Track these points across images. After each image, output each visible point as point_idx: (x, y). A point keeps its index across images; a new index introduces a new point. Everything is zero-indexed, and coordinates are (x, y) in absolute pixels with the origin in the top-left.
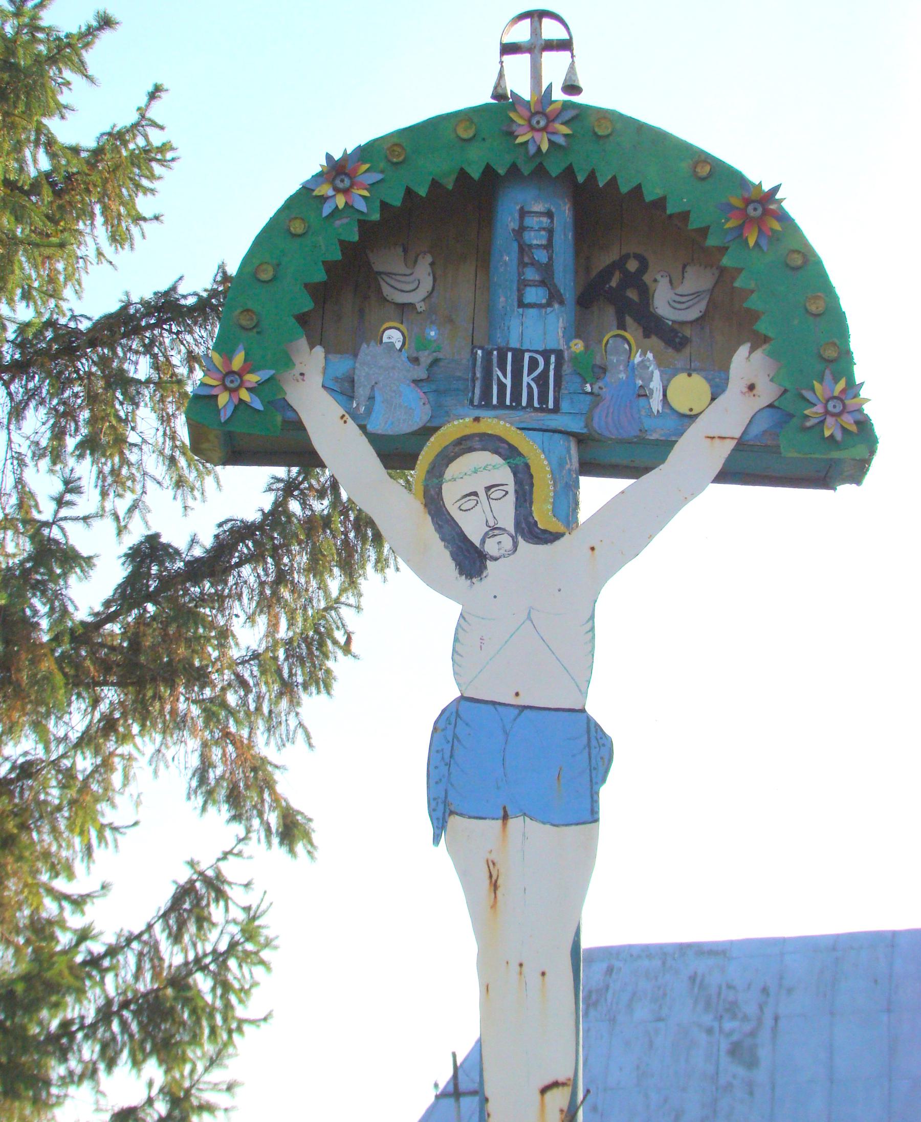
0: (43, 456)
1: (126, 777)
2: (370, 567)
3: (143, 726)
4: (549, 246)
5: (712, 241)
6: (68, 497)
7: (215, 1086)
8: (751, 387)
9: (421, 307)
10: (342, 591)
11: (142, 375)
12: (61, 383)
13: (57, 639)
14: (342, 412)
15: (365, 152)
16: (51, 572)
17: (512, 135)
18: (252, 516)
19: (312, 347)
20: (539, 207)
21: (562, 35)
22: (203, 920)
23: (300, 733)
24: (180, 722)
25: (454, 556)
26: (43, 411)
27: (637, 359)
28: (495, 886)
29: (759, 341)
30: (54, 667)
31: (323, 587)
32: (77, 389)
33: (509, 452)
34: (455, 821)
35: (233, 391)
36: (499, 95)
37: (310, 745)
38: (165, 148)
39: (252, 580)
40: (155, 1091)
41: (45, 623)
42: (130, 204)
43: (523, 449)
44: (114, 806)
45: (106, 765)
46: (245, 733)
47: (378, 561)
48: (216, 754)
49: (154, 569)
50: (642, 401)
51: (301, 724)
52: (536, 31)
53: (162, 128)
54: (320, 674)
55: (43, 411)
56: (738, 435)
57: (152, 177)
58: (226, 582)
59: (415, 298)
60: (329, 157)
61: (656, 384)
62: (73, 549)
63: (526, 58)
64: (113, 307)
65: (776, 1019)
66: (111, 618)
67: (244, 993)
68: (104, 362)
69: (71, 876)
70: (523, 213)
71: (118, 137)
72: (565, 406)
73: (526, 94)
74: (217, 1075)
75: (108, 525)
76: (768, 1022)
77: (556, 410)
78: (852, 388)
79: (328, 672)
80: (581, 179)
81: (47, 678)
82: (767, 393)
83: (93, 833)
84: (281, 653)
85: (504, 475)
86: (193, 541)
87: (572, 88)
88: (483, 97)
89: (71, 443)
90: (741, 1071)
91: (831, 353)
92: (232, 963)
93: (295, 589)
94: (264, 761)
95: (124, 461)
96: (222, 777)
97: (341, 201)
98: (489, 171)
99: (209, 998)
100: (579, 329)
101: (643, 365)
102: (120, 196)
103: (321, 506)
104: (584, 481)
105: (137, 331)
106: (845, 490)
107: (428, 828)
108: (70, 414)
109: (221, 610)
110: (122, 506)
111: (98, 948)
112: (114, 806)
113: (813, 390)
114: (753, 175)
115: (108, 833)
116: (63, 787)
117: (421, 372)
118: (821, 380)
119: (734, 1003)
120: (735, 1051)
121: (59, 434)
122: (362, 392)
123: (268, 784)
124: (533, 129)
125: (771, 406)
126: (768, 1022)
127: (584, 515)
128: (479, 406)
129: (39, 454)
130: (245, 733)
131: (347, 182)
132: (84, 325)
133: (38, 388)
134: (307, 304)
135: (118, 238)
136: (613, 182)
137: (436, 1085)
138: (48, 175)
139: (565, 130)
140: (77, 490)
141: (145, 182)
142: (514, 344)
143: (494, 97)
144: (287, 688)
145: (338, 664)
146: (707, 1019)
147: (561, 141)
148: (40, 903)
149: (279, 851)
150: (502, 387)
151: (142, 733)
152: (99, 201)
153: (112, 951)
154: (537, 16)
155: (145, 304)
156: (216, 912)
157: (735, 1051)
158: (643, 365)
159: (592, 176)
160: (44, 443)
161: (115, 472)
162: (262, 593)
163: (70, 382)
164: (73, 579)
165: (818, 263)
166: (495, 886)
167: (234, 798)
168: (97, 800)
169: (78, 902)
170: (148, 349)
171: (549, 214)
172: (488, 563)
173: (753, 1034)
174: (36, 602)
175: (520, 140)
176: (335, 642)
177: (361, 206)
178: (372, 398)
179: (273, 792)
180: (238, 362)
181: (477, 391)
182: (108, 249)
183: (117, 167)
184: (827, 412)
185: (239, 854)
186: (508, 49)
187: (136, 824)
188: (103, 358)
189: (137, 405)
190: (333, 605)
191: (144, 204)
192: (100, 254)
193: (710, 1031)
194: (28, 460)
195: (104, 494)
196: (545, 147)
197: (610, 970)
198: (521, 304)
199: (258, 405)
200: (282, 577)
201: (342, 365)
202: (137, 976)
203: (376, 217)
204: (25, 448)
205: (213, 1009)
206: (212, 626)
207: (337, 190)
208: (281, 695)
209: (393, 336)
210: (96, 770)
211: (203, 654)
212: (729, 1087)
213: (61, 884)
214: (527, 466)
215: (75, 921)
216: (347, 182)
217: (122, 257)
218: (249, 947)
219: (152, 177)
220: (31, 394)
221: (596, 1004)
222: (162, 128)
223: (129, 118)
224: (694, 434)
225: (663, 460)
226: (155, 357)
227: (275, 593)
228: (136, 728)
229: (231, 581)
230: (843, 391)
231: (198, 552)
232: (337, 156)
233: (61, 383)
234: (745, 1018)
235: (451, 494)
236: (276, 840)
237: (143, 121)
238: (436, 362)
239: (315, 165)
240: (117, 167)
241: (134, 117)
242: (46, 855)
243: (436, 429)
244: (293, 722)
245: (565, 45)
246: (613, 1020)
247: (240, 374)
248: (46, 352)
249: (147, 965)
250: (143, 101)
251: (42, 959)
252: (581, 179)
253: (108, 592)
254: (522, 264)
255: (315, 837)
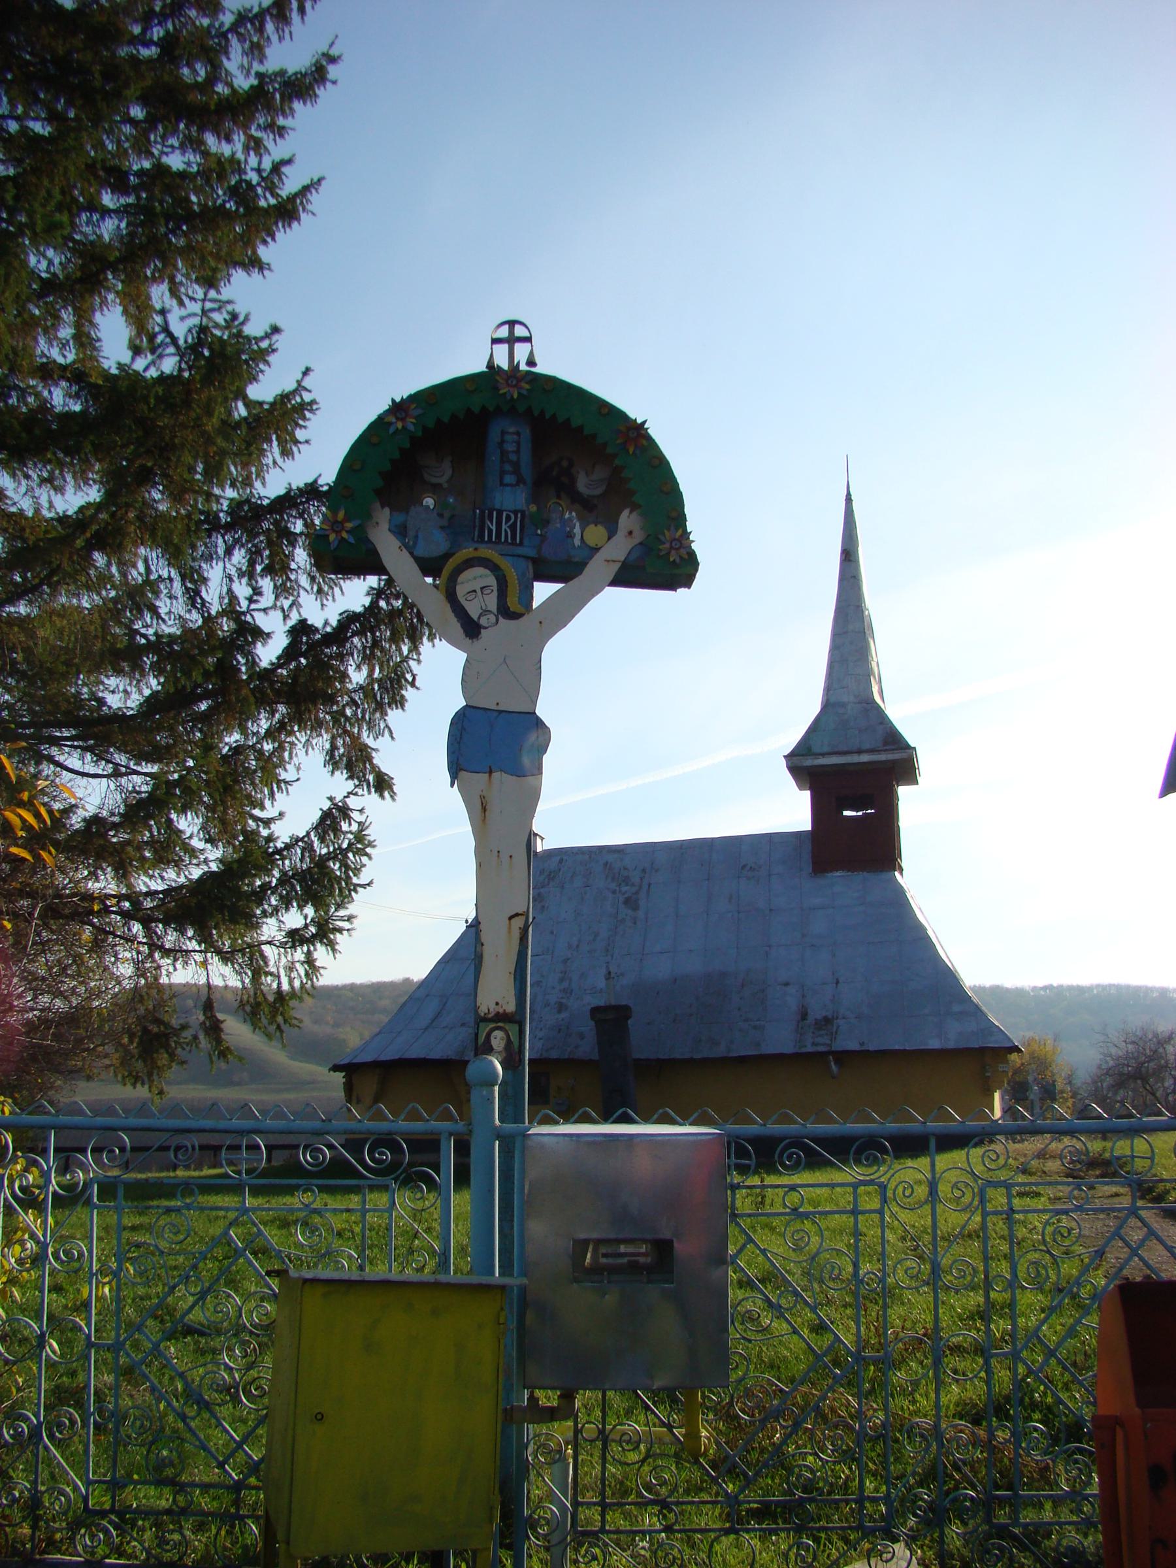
0: (243, 576)
1: (291, 754)
2: (425, 639)
3: (300, 726)
4: (518, 452)
5: (610, 450)
6: (255, 598)
7: (342, 919)
8: (630, 533)
9: (445, 485)
10: (410, 651)
11: (298, 531)
12: (252, 535)
13: (250, 677)
14: (399, 544)
15: (414, 398)
16: (246, 639)
17: (496, 389)
18: (359, 609)
19: (383, 507)
20: (512, 430)
21: (525, 334)
22: (337, 830)
23: (387, 733)
24: (318, 725)
25: (462, 626)
26: (243, 551)
27: (567, 516)
28: (484, 809)
29: (634, 507)
30: (249, 693)
31: (399, 650)
32: (262, 538)
33: (494, 568)
34: (463, 774)
35: (338, 532)
36: (490, 365)
37: (393, 738)
38: (313, 402)
39: (359, 645)
40: (309, 921)
41: (244, 669)
42: (292, 435)
43: (503, 567)
44: (286, 770)
45: (281, 748)
46: (356, 731)
47: (430, 635)
48: (340, 742)
49: (304, 639)
50: (569, 540)
51: (387, 726)
52: (511, 331)
53: (310, 391)
54: (398, 698)
55: (243, 551)
56: (622, 559)
57: (304, 418)
58: (344, 647)
59: (444, 481)
60: (393, 400)
61: (577, 530)
62: (259, 627)
63: (505, 347)
64: (282, 492)
65: (649, 885)
66: (280, 666)
67: (357, 871)
68: (276, 523)
69: (263, 808)
70: (503, 433)
71: (284, 398)
72: (526, 542)
73: (505, 366)
74: (342, 913)
75: (278, 615)
76: (645, 887)
77: (521, 544)
78: (686, 534)
79: (403, 697)
80: (536, 413)
81: (246, 699)
82: (639, 536)
83: (275, 786)
84: (376, 687)
85: (491, 581)
86: (326, 623)
87: (531, 362)
88: (481, 367)
89: (259, 568)
90: (630, 912)
91: (674, 514)
92: (350, 855)
93: (383, 650)
94: (366, 746)
95: (289, 579)
96: (343, 755)
97: (400, 425)
98: (484, 409)
99: (338, 873)
100: (534, 498)
101: (570, 519)
102: (287, 429)
103: (398, 604)
104: (536, 584)
105: (295, 505)
106: (682, 591)
107: (447, 778)
108: (258, 552)
109: (342, 661)
110: (286, 604)
111: (280, 845)
112: (286, 770)
113: (664, 534)
114: (632, 416)
115: (283, 785)
116: (257, 759)
117: (445, 523)
118: (669, 530)
119: (627, 877)
120: (627, 902)
121: (252, 563)
122: (411, 533)
123: (370, 759)
124: (508, 385)
125: (641, 544)
126: (645, 887)
127: (535, 605)
128: (477, 542)
129: (241, 574)
130: (356, 731)
131: (404, 415)
132: (266, 502)
133: (240, 538)
134: (380, 483)
135: (286, 453)
136: (554, 416)
137: (467, 921)
138: (245, 419)
139: (527, 387)
140: (260, 594)
141: (301, 422)
142: (498, 506)
143: (488, 367)
144: (380, 707)
145: (409, 693)
146: (613, 886)
147: (525, 392)
148: (246, 823)
149: (374, 796)
150: (490, 531)
151: (299, 730)
152: (276, 433)
153: (288, 847)
154: (512, 324)
155: (299, 489)
156: (345, 826)
157: (627, 902)
158: (570, 519)
159: (542, 413)
160: (244, 569)
161: (284, 584)
162: (364, 652)
163: (258, 534)
164: (259, 645)
165: (668, 463)
166: (484, 809)
167: (350, 767)
168: (276, 767)
169: (267, 822)
170: (301, 516)
171: (518, 434)
172: (483, 631)
173: (637, 893)
174: (239, 658)
175: (502, 392)
176: (406, 680)
177: (412, 428)
178: (416, 537)
179: (371, 763)
180: (341, 515)
181: (476, 533)
182: (279, 460)
183: (285, 413)
184: (671, 548)
185: (356, 794)
186: (495, 341)
187: (298, 780)
188: (276, 520)
189: (294, 547)
190: (405, 659)
191: (300, 434)
192: (275, 462)
193: (614, 892)
194: (235, 579)
195: (277, 598)
196: (515, 396)
197: (561, 861)
198: (502, 484)
199: (352, 540)
200: (376, 643)
201: (400, 518)
202: (302, 860)
203: (420, 434)
204: (233, 572)
205: (340, 878)
206: (337, 671)
207: (397, 419)
208: (375, 710)
209: (429, 502)
210: (275, 750)
211: (332, 686)
212: (623, 921)
213: (257, 812)
214: (505, 576)
215: (265, 832)
216: (404, 415)
217: (288, 464)
218: (359, 846)
219: (304, 418)
220: (237, 541)
221: (553, 879)
222: (310, 391)
223: (293, 386)
224: (599, 557)
225: (581, 573)
226: (304, 519)
227: (372, 653)
228: (296, 728)
229: (348, 645)
230: (681, 536)
231: (329, 629)
232: (398, 400)
233: (252, 535)
234: (633, 885)
235: (461, 591)
236: (373, 790)
237: (301, 387)
238: (453, 516)
239: (384, 406)
240: (285, 413)
241: (294, 386)
242: (249, 796)
243: (453, 554)
244: (382, 725)
245: (528, 340)
246: (563, 887)
247: (342, 523)
248: (245, 518)
249: (307, 855)
250: (299, 376)
251: (248, 853)
252: (536, 413)
253: (279, 651)
254: (502, 462)
255: (395, 788)
